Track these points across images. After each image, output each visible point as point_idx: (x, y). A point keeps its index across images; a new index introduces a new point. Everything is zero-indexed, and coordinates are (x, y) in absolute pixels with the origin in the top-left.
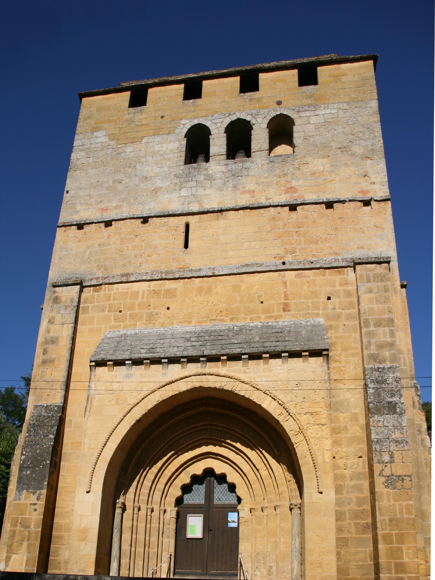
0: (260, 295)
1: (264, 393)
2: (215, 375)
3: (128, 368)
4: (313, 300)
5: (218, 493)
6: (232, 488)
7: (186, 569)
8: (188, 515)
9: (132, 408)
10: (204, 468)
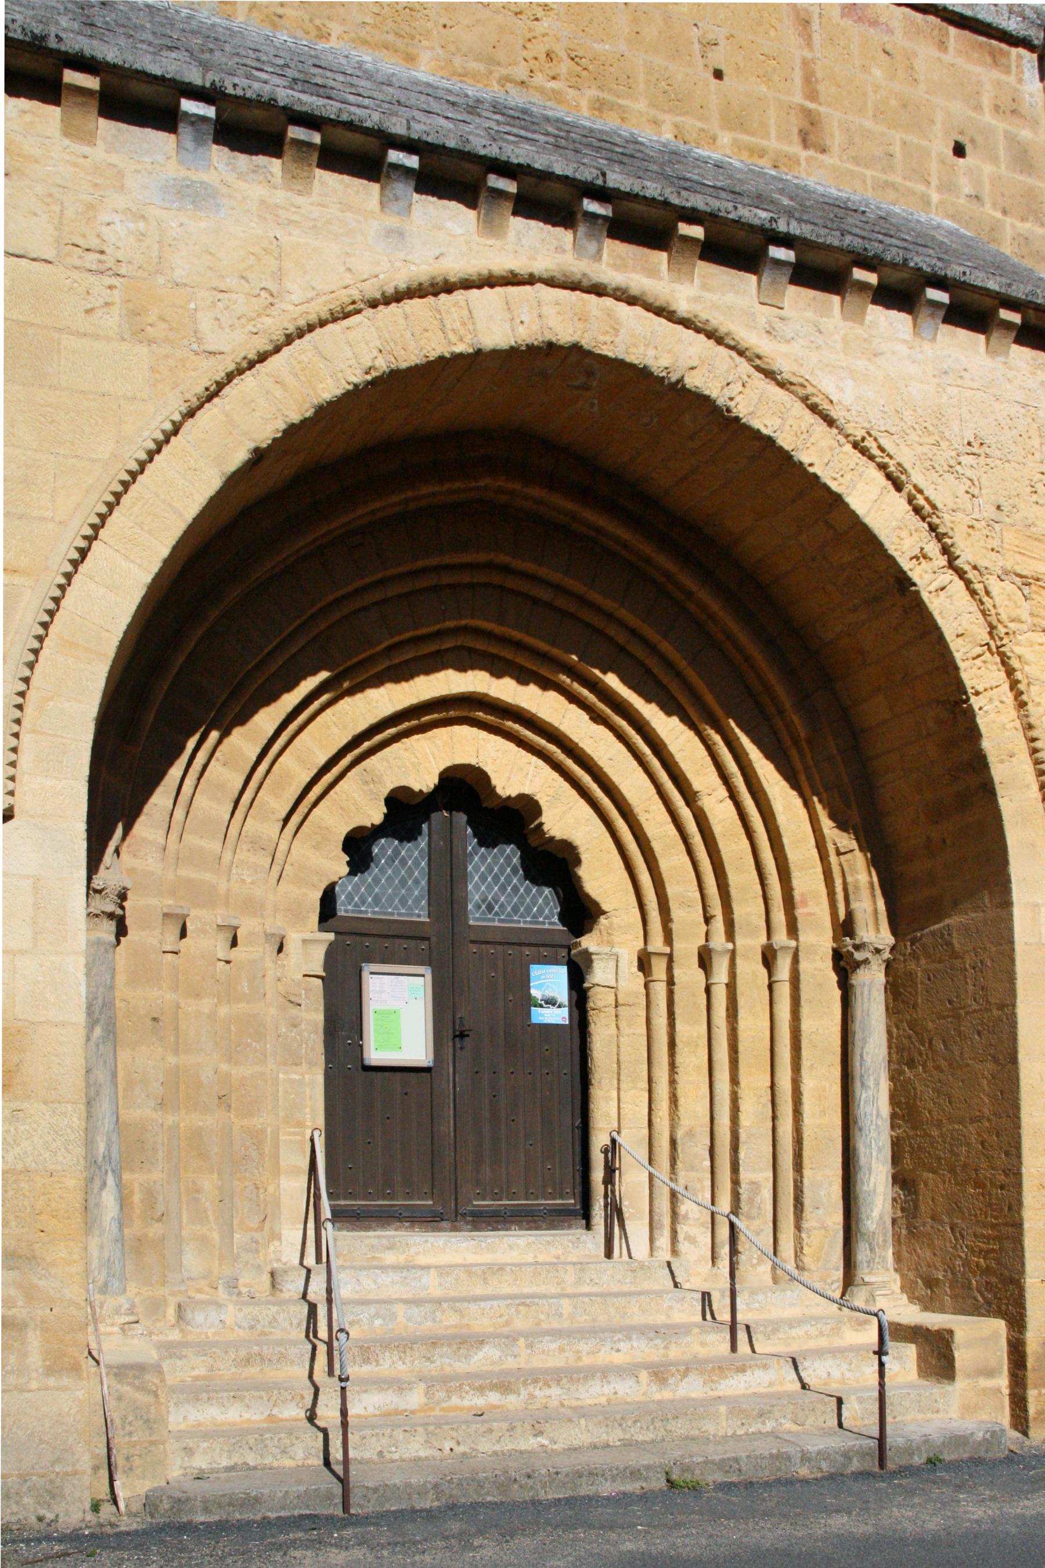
0: (711, 36)
1: (855, 445)
2: (648, 307)
3: (189, 144)
4: (908, 138)
5: (483, 878)
6: (553, 866)
7: (368, 1196)
8: (367, 968)
9: (230, 377)
10: (442, 768)
